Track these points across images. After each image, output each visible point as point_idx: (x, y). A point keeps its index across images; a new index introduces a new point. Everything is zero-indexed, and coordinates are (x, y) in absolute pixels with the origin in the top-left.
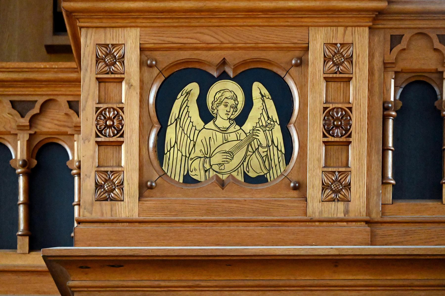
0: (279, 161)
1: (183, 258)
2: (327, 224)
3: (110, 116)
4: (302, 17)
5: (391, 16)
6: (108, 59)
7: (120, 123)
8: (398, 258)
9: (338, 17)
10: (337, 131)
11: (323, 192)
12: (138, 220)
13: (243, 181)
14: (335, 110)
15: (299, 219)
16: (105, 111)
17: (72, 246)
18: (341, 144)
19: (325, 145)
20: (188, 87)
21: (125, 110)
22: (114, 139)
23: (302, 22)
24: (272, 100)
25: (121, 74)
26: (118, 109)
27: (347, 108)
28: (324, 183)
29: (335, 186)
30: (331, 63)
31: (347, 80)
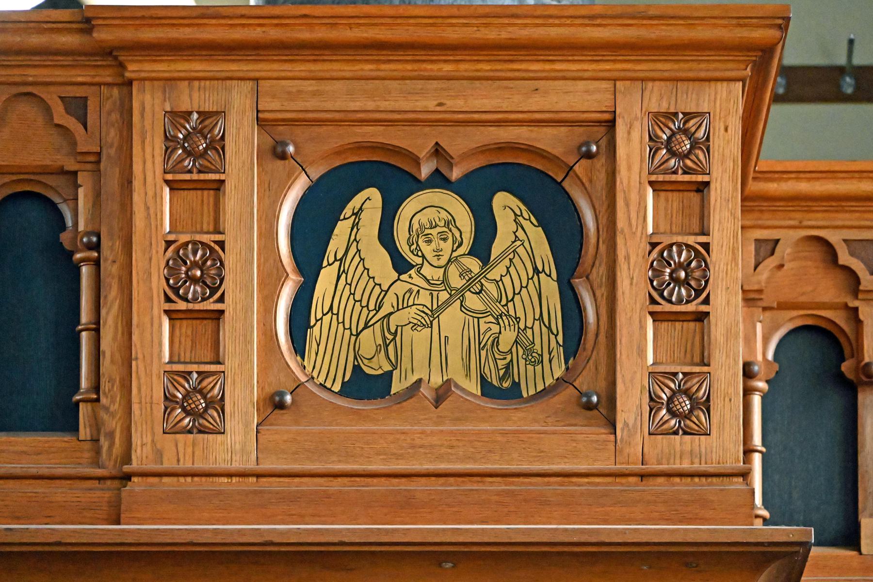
0: (551, 350)
1: (84, 549)
2: (241, 480)
3: (679, 262)
4: (424, 61)
5: (180, 53)
6: (684, 148)
7: (658, 273)
8: (705, 549)
9: (315, 60)
10: (193, 290)
11: (166, 415)
12: (513, 471)
13: (479, 393)
14: (190, 246)
15: (481, 471)
16: (186, 249)
17: (119, 523)
18: (196, 315)
19: (170, 319)
20: (356, 202)
21: (227, 246)
22: (691, 307)
23: (426, 70)
24: (540, 228)
25: (220, 173)
26: (212, 244)
27: (215, 242)
28: (653, 396)
29: (683, 404)
30: (665, 151)
31: (215, 186)
